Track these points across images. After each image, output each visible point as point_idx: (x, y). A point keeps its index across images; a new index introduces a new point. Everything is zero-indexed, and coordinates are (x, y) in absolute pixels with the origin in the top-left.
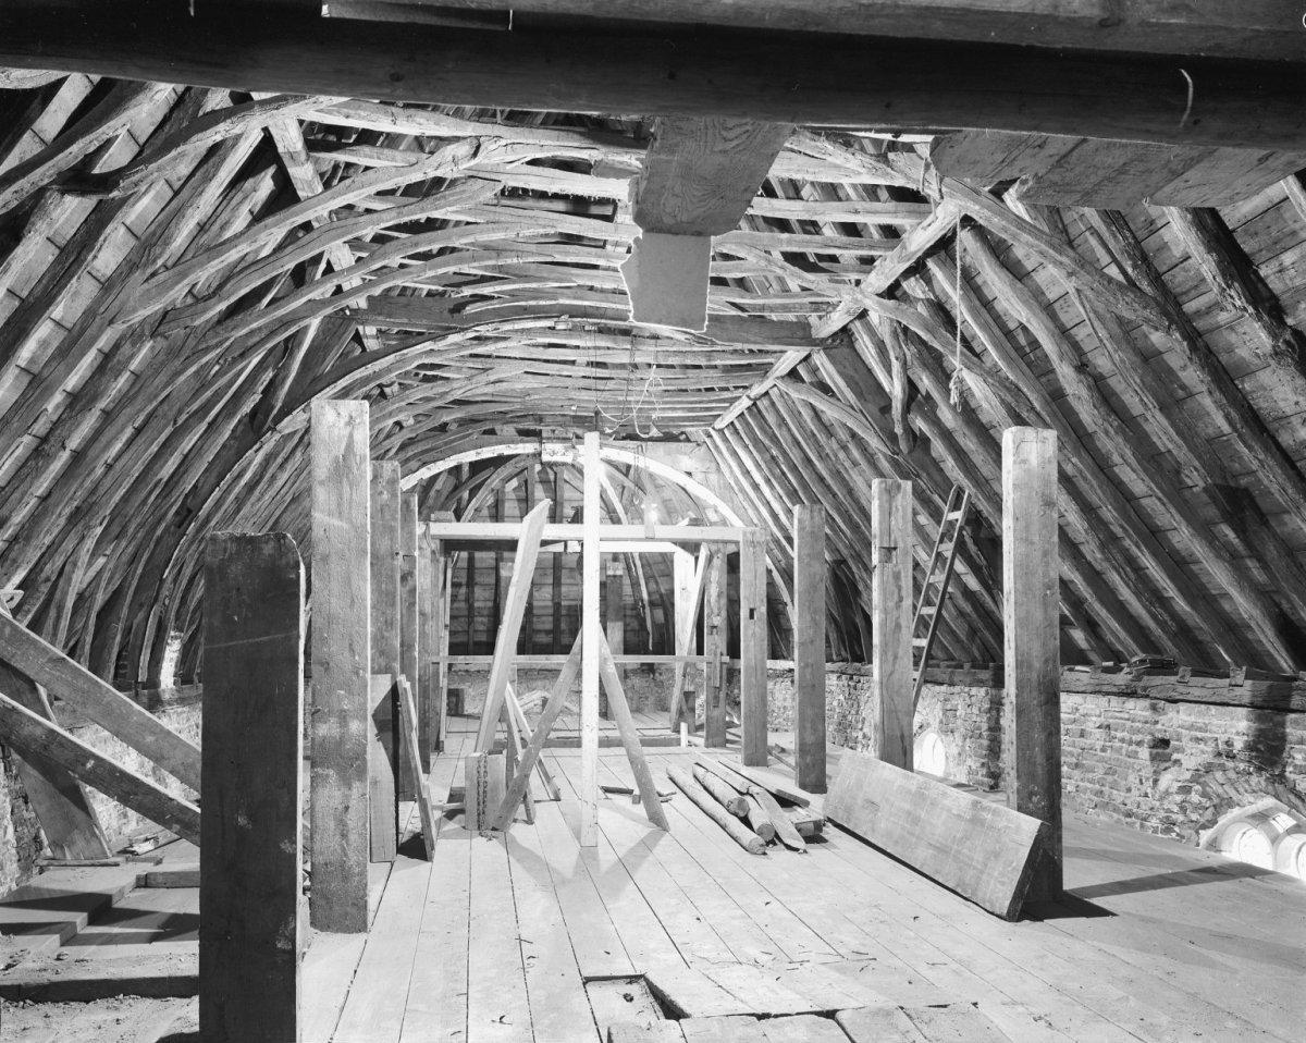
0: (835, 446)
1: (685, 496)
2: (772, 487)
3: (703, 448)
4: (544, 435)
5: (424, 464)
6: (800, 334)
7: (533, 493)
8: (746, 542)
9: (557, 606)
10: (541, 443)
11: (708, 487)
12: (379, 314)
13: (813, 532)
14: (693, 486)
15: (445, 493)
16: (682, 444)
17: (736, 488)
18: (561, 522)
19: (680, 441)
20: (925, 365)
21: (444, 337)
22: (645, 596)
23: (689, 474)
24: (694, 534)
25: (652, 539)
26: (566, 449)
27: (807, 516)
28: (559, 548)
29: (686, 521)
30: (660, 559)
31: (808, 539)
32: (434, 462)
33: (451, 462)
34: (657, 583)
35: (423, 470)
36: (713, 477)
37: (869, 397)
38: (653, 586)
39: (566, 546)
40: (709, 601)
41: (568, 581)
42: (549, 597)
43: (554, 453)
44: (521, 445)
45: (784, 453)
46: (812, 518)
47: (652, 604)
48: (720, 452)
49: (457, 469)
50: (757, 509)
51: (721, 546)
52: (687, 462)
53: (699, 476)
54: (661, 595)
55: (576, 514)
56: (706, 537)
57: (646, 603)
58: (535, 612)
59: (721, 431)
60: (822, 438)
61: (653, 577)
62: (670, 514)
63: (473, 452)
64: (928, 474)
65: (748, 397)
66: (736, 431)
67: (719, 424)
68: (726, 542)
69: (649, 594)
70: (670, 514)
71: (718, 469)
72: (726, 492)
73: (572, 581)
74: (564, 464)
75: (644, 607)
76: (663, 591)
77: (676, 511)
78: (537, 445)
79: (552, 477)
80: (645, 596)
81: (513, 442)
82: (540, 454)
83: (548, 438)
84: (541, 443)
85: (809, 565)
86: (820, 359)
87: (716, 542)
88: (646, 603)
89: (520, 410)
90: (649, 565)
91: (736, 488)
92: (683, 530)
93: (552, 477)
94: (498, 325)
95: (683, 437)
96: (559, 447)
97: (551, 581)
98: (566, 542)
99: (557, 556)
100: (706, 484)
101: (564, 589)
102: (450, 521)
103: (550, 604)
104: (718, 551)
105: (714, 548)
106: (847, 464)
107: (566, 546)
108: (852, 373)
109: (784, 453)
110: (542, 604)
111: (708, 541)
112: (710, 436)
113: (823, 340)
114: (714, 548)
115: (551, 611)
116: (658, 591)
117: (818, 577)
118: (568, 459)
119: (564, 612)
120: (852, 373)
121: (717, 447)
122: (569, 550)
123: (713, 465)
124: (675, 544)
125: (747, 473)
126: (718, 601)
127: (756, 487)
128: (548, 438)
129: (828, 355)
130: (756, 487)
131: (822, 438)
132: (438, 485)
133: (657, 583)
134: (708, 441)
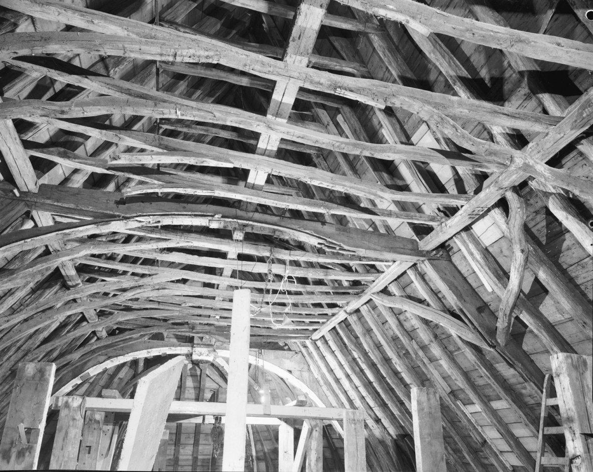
0: (416, 347)
1: (284, 386)
2: (350, 380)
3: (300, 355)
4: (195, 341)
5: (109, 358)
6: (410, 246)
7: (185, 382)
8: (349, 420)
9: (195, 459)
10: (193, 347)
11: (303, 381)
12: (48, 198)
13: (430, 413)
14: (292, 380)
15: (126, 380)
16: (286, 352)
17: (322, 382)
18: (203, 401)
19: (284, 350)
20: (541, 261)
21: (107, 222)
22: (254, 453)
23: (290, 372)
24: (298, 412)
25: (269, 415)
26: (209, 352)
27: (424, 398)
28: (199, 420)
29: (295, 402)
30: (265, 429)
31: (427, 419)
32: (117, 356)
33: (128, 358)
34: (262, 445)
35: (108, 362)
36: (306, 374)
37: (467, 299)
38: (259, 446)
39: (204, 419)
40: (310, 465)
41: (204, 442)
42: (190, 453)
43: (201, 354)
44: (179, 348)
45: (365, 354)
46: (429, 400)
47: (258, 459)
48: (312, 357)
49: (135, 362)
50: (336, 396)
51: (318, 421)
52: (289, 364)
53: (297, 373)
54: (265, 453)
55: (213, 396)
56: (308, 415)
57: (254, 458)
58: (180, 463)
59: (314, 342)
60: (404, 340)
61: (260, 440)
62: (275, 398)
63: (145, 351)
64: (522, 364)
65: (345, 311)
66: (326, 342)
67: (316, 336)
68: (322, 419)
69: (257, 452)
70: (275, 398)
71: (309, 369)
72: (314, 384)
73: (207, 442)
74: (207, 362)
75: (252, 461)
76: (266, 450)
77: (278, 397)
78: (190, 349)
79: (198, 373)
80: (254, 453)
81: (173, 346)
82: (191, 355)
83: (198, 344)
84: (193, 347)
85: (430, 444)
86: (427, 267)
87: (315, 418)
88: (254, 458)
89: (178, 317)
90: (258, 432)
91: (322, 382)
92: (290, 409)
93: (198, 373)
94: (159, 218)
95: (286, 348)
96: (204, 350)
97: (193, 442)
98: (204, 416)
99: (198, 426)
100: (301, 378)
101: (200, 448)
102: (114, 397)
103: (191, 457)
104: (316, 426)
105: (313, 423)
106: (426, 360)
107: (204, 419)
108: (452, 279)
109: (365, 354)
110: (185, 457)
111: (309, 418)
112: (305, 347)
113: (428, 252)
114: (313, 423)
115: (190, 463)
116: (263, 450)
117: (439, 455)
118: (210, 359)
119: (199, 463)
120: (452, 279)
121: (310, 354)
122: (206, 422)
123: (306, 367)
124: (280, 419)
125: (331, 371)
126: (316, 465)
127: (337, 381)
128: (198, 344)
129: (432, 264)
130: (337, 381)
131: (404, 340)
132: (122, 374)
133: (262, 445)
134: (303, 350)
